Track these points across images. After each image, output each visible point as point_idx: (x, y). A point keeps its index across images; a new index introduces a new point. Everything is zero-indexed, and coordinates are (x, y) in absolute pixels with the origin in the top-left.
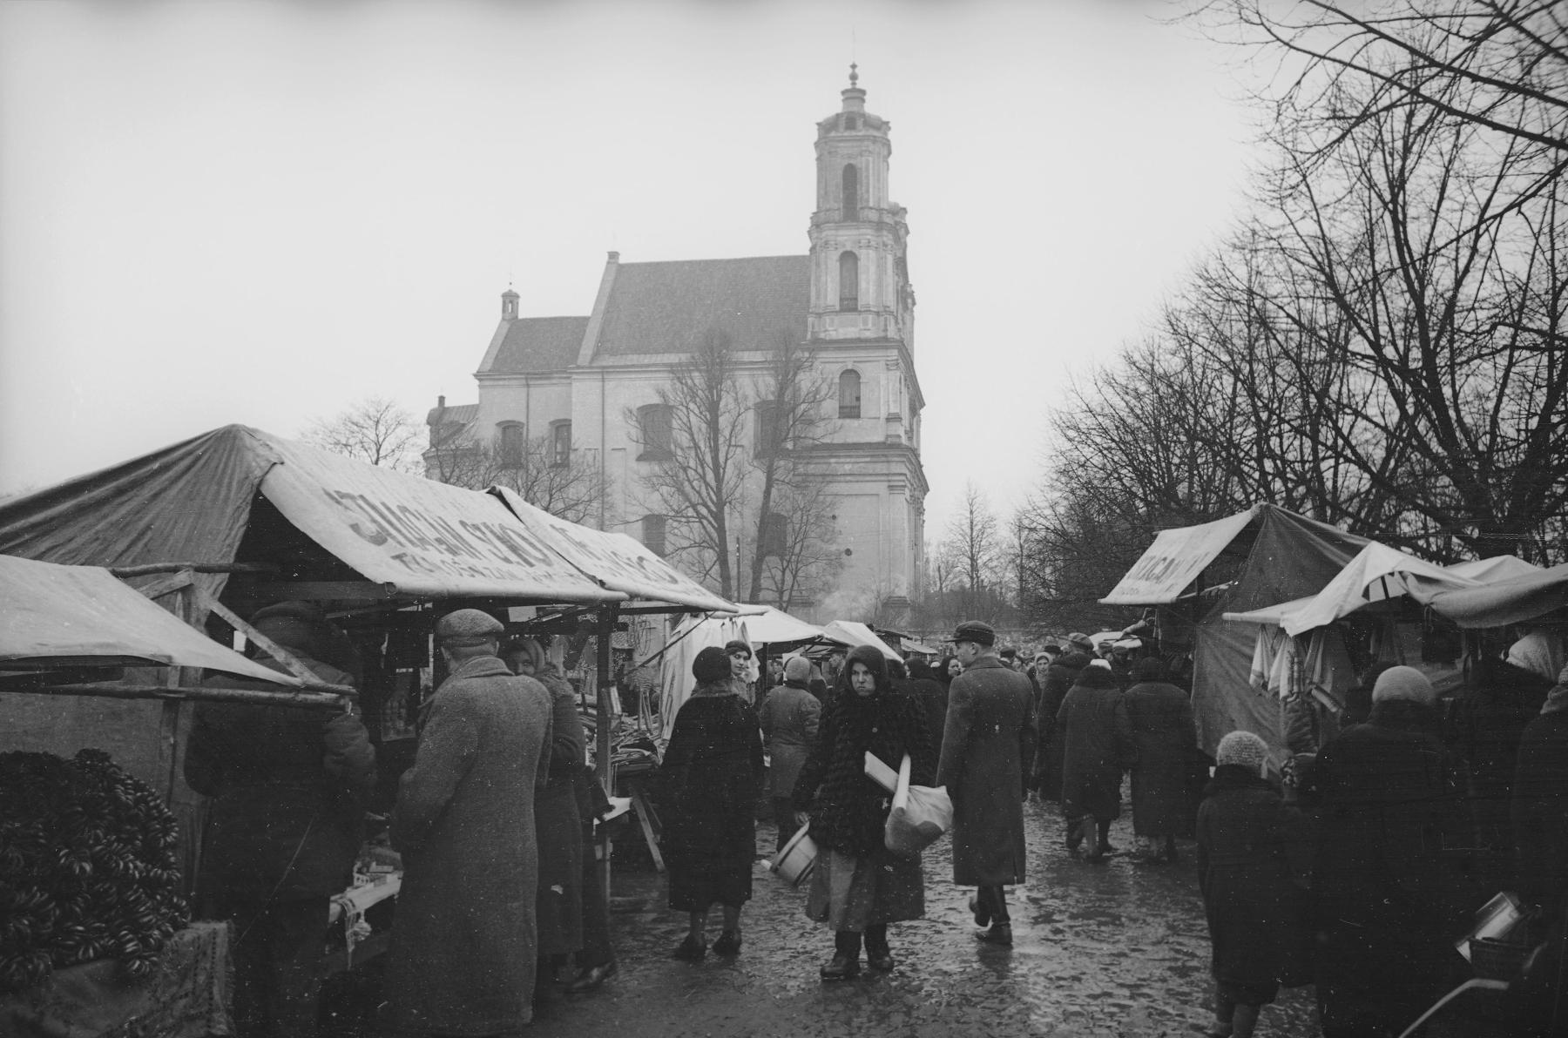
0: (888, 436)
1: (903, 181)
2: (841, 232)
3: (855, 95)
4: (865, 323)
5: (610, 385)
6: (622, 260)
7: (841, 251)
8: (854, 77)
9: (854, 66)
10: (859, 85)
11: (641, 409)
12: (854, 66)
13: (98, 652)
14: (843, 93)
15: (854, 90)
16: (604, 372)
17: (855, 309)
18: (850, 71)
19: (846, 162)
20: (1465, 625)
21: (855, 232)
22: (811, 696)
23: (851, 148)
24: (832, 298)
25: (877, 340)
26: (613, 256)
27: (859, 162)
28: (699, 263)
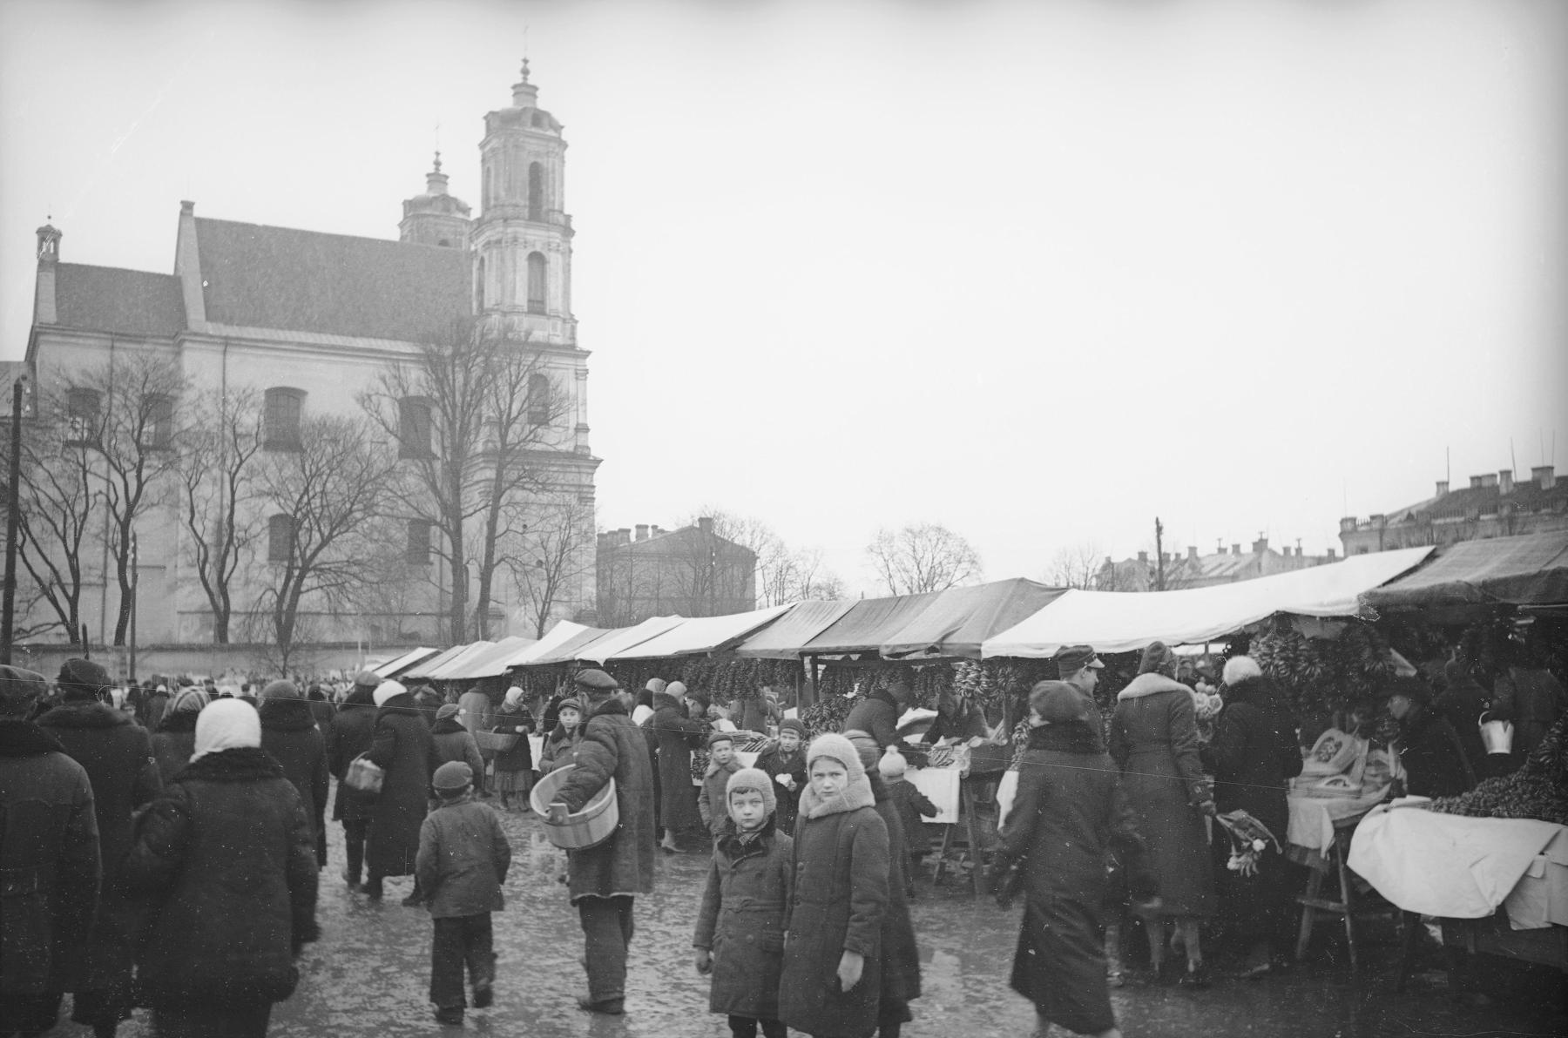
0: (576, 447)
1: (580, 189)
2: (530, 231)
3: (525, 90)
4: (554, 328)
5: (233, 359)
6: (198, 212)
7: (530, 250)
8: (525, 72)
9: (526, 61)
10: (531, 81)
11: (269, 392)
12: (526, 61)
13: (1117, 651)
14: (515, 87)
15: (524, 85)
16: (227, 343)
17: (542, 313)
18: (521, 65)
19: (532, 159)
20: (1178, 651)
21: (543, 233)
22: (1239, 704)
23: (524, 142)
24: (521, 299)
25: (564, 347)
26: (187, 206)
27: (545, 162)
28: (296, 232)
